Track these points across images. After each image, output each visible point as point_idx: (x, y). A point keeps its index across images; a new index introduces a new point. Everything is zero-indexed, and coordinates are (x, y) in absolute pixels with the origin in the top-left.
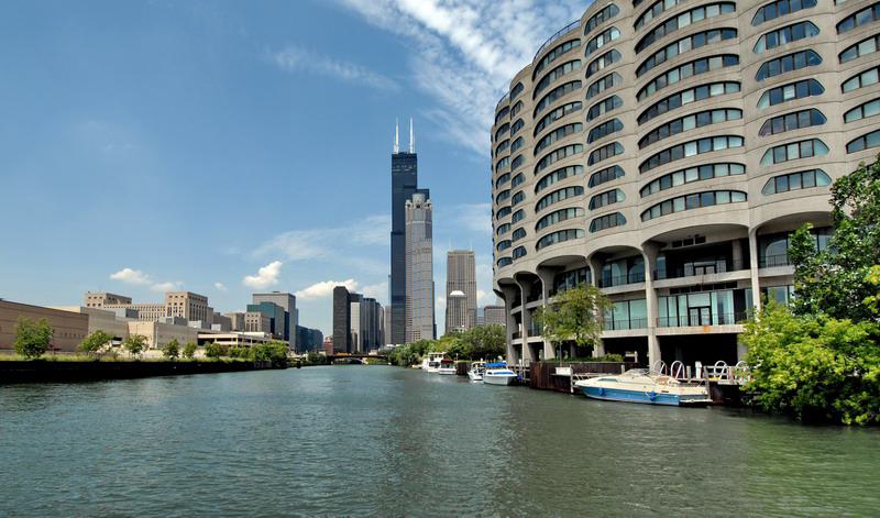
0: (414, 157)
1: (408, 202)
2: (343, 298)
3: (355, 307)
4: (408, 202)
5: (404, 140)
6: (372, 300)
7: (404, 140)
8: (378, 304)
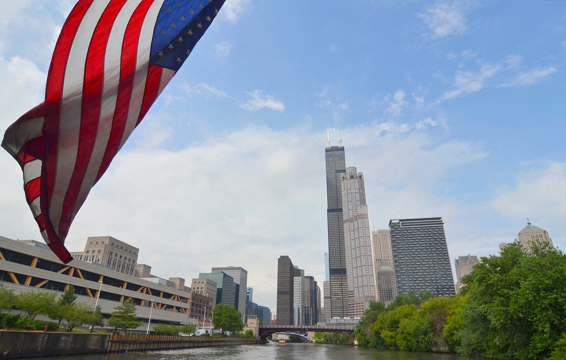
3: (297, 280)
6: (312, 278)
8: (316, 283)
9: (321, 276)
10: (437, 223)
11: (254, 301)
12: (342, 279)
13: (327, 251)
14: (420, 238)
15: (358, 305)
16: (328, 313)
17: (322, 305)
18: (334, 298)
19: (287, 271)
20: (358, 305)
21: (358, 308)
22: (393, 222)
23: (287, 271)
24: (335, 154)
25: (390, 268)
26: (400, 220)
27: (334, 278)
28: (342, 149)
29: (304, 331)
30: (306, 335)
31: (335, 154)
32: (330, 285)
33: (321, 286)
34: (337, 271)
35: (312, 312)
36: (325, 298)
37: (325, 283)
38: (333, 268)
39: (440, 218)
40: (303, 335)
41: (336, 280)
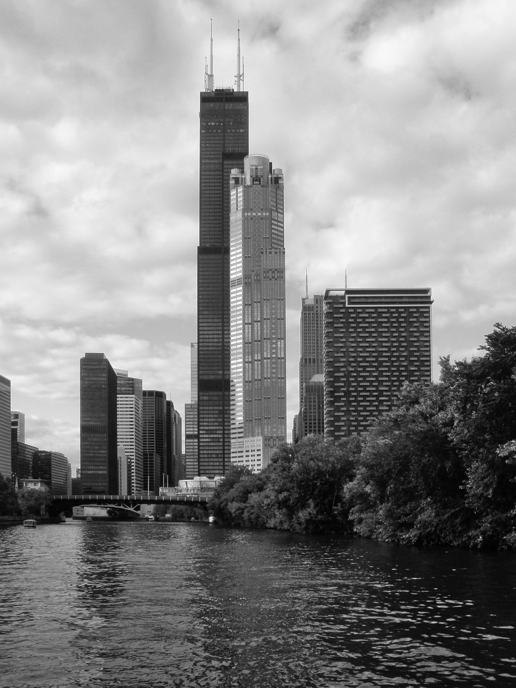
1: (234, 172)
4: (234, 172)
6: (160, 395)
8: (170, 404)
10: (421, 298)
11: (29, 441)
12: (224, 426)
14: (377, 327)
15: (308, 425)
16: (191, 464)
17: (183, 452)
18: (205, 438)
19: (101, 384)
20: (250, 453)
22: (332, 293)
23: (101, 384)
24: (224, 114)
25: (320, 378)
26: (348, 292)
27: (206, 398)
28: (242, 98)
29: (136, 503)
30: (138, 509)
31: (224, 114)
32: (200, 409)
33: (180, 409)
34: (213, 383)
35: (160, 457)
36: (188, 437)
37: (188, 408)
38: (189, 433)
39: (426, 291)
40: (131, 509)
41: (206, 312)
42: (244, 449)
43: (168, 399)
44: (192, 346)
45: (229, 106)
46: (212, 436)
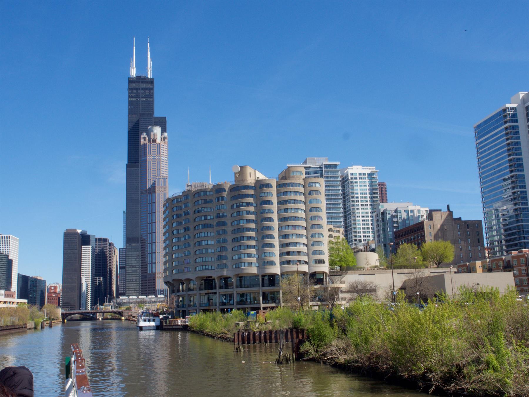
0: (151, 81)
2: (74, 241)
5: (141, 64)
6: (105, 240)
7: (141, 64)
9: (118, 240)
13: (125, 210)
15: (150, 281)
20: (150, 281)
21: (150, 284)
24: (448, 206)
42: (147, 279)
43: (110, 241)
44: (124, 212)
45: (144, 86)
46: (133, 269)
